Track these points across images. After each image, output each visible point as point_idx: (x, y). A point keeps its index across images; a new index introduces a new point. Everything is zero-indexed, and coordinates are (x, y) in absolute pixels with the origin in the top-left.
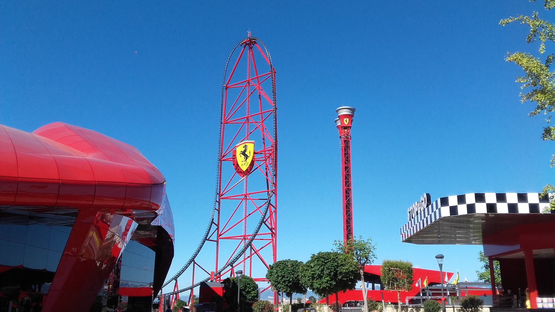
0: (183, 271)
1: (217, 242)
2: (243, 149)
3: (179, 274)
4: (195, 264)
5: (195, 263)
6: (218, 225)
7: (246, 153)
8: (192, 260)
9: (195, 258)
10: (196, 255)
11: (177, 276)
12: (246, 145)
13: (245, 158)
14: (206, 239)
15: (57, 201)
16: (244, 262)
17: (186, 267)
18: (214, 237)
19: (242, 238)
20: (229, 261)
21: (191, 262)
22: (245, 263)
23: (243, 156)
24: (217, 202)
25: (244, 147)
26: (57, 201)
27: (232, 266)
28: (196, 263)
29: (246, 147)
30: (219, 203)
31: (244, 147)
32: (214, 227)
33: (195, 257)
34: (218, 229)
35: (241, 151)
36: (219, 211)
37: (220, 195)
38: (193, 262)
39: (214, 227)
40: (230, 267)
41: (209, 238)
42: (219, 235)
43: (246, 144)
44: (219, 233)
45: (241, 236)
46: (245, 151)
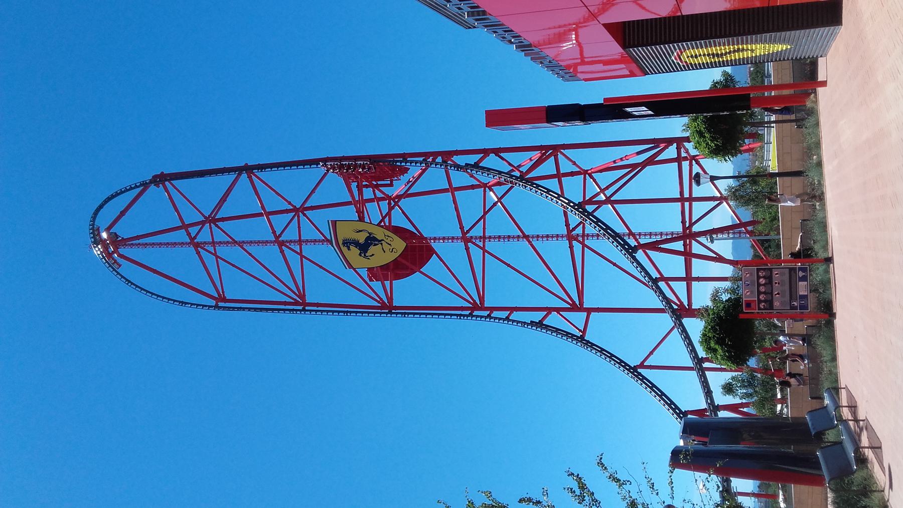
0: (662, 395)
1: (589, 311)
2: (355, 250)
3: (622, 363)
4: (645, 364)
5: (642, 365)
6: (549, 310)
7: (362, 241)
8: (634, 371)
9: (629, 366)
10: (622, 363)
11: (674, 410)
12: (344, 244)
13: (375, 245)
14: (581, 339)
15: (846, 407)
16: (638, 237)
17: (652, 387)
18: (578, 318)
19: (577, 247)
20: (643, 279)
21: (640, 374)
22: (640, 234)
23: (372, 250)
24: (492, 315)
25: (349, 249)
26: (846, 407)
27: (635, 249)
28: (642, 363)
29: (347, 243)
30: (492, 309)
31: (349, 249)
32: (554, 320)
33: (626, 364)
34: (558, 310)
35: (360, 255)
36: (512, 310)
37: (475, 307)
38: (639, 370)
39: (554, 320)
40: (640, 255)
41: (580, 330)
42: (575, 308)
43: (341, 242)
44: (569, 306)
45: (571, 247)
46: (356, 244)
